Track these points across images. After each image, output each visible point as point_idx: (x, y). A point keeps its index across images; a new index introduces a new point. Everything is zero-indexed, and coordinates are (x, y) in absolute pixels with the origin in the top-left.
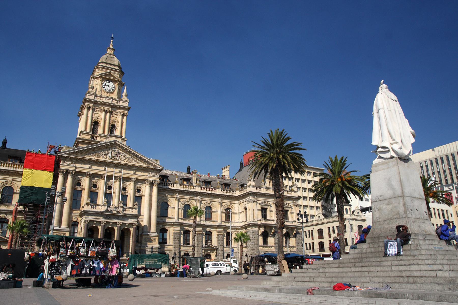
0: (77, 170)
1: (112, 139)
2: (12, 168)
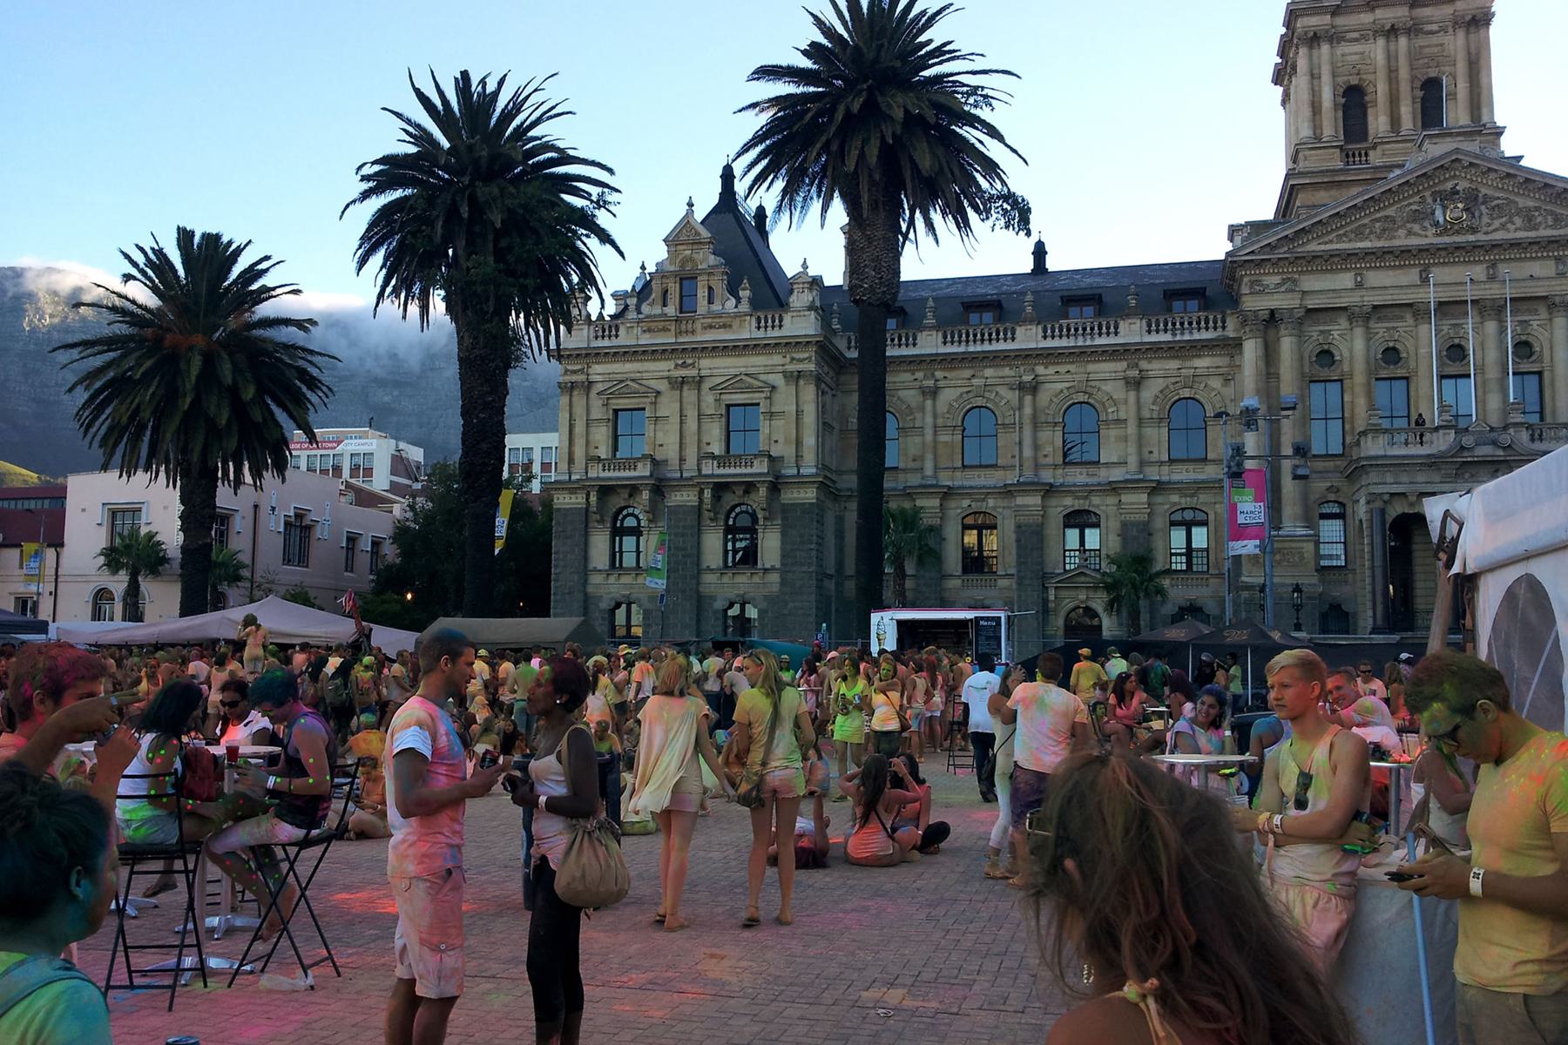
0: (1311, 303)
1: (1437, 149)
2: (1080, 339)
